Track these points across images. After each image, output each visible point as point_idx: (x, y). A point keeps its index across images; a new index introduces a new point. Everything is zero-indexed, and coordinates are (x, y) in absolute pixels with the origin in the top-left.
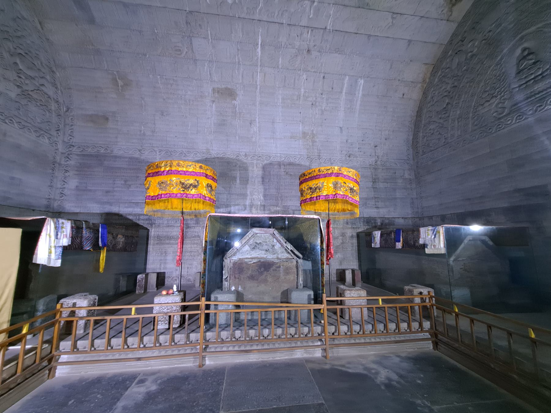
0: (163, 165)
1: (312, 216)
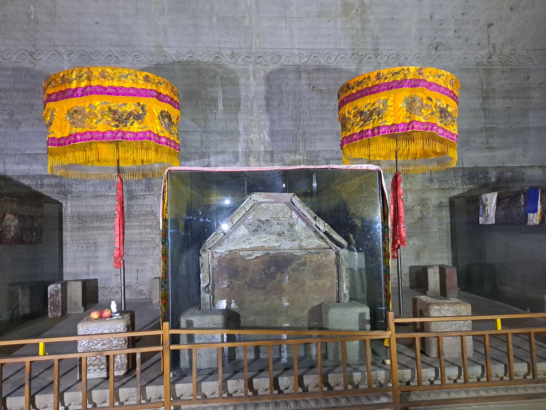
0: (74, 76)
1: (365, 167)
